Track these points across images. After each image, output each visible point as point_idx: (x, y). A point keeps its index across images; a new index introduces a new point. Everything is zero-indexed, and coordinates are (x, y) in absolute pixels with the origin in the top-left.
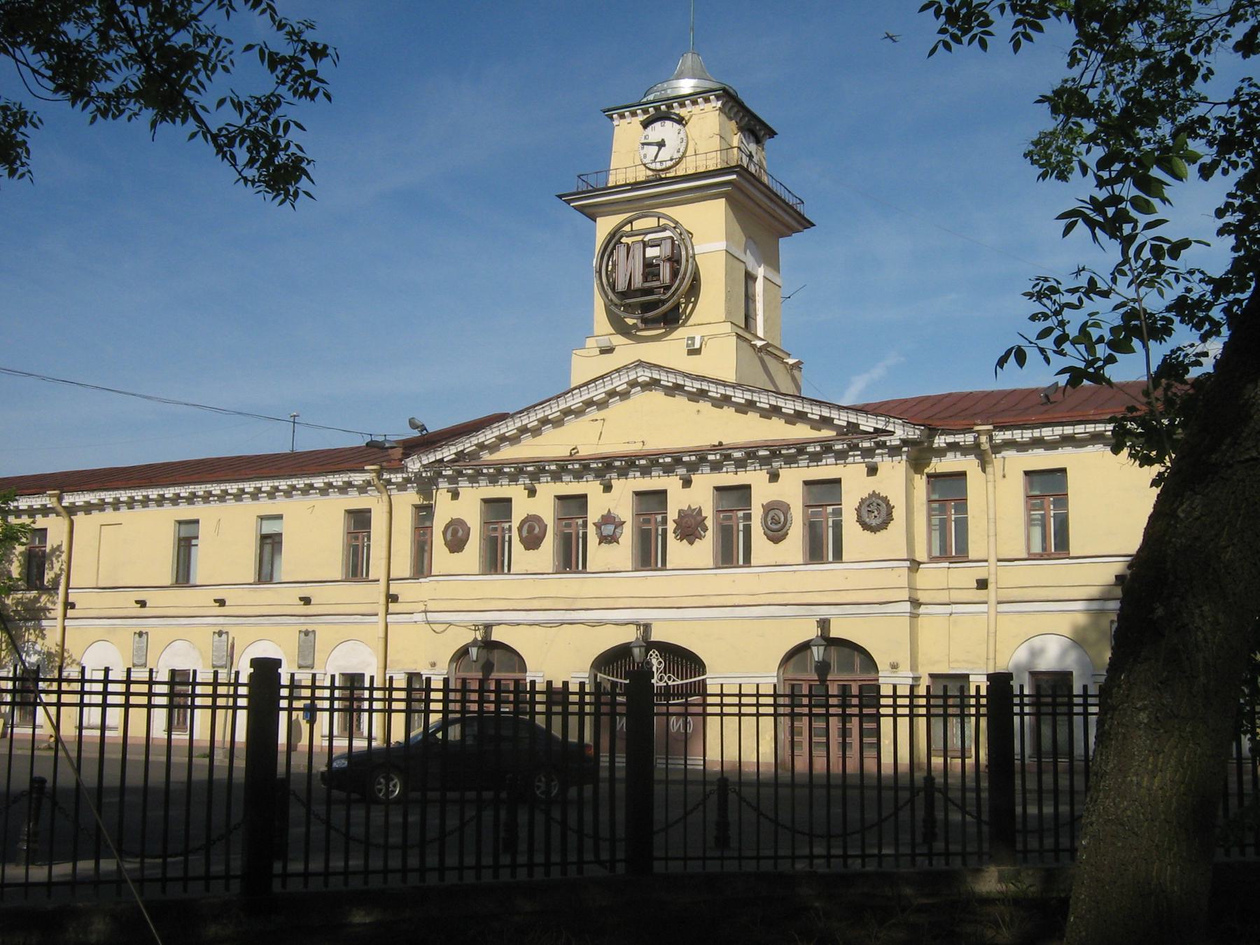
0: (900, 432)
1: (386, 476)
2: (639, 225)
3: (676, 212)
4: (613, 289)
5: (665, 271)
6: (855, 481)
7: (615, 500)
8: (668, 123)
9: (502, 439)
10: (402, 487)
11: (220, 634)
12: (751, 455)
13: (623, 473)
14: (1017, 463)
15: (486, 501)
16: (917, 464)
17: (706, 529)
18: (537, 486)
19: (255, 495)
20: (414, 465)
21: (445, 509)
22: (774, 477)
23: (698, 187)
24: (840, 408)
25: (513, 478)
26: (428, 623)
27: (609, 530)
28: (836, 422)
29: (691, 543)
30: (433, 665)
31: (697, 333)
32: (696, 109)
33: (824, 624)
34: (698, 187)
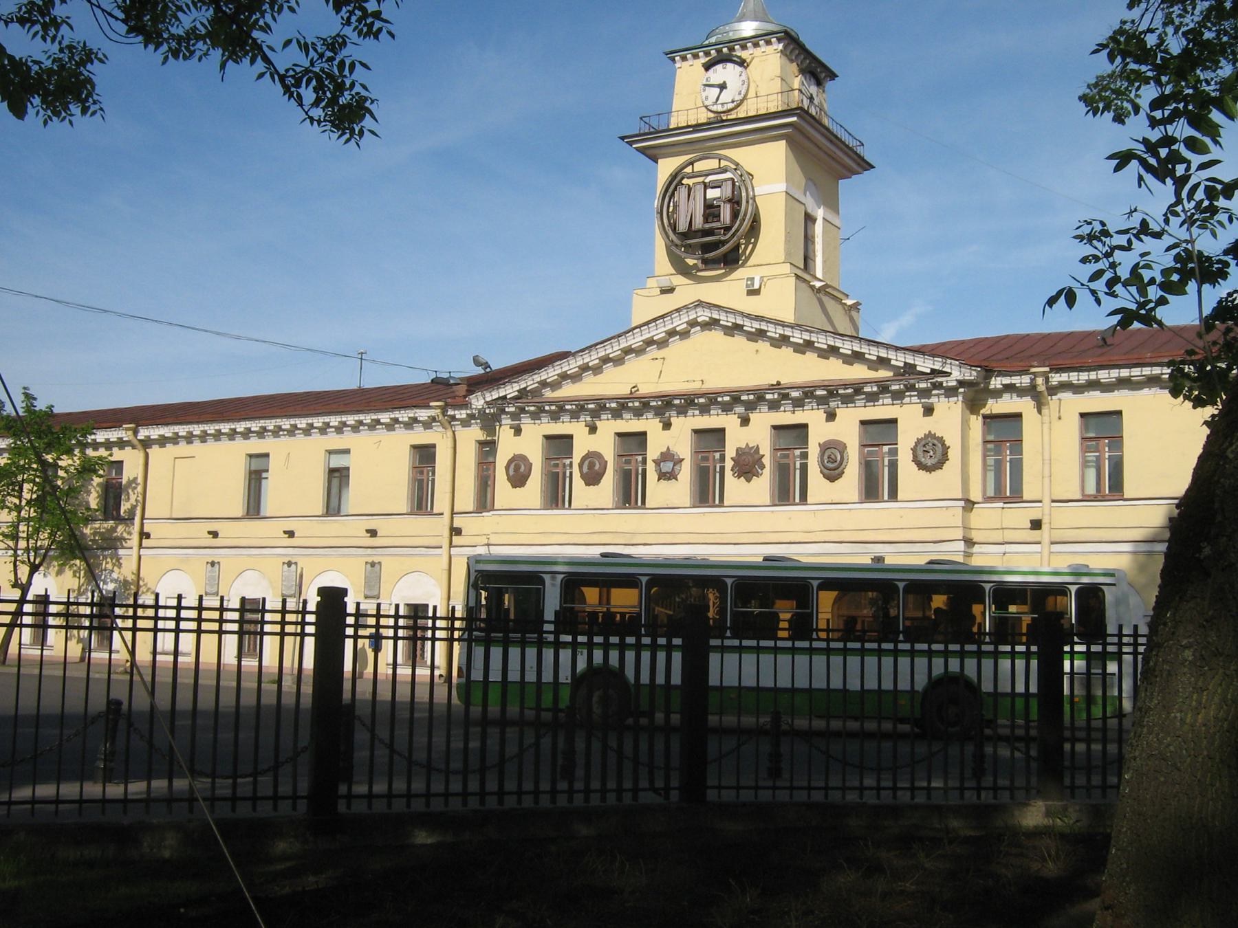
1: (450, 412)
2: (700, 166)
3: (736, 154)
4: (674, 230)
5: (726, 213)
6: (911, 423)
7: (673, 438)
8: (730, 65)
9: (564, 377)
10: (466, 423)
11: (289, 564)
12: (807, 394)
13: (682, 411)
14: (1072, 405)
15: (548, 438)
16: (973, 405)
19: (323, 430)
20: (478, 401)
21: (507, 445)
22: (831, 416)
23: (758, 129)
24: (897, 349)
25: (575, 415)
28: (893, 362)
29: (748, 480)
31: (757, 274)
32: (758, 52)
34: (758, 129)
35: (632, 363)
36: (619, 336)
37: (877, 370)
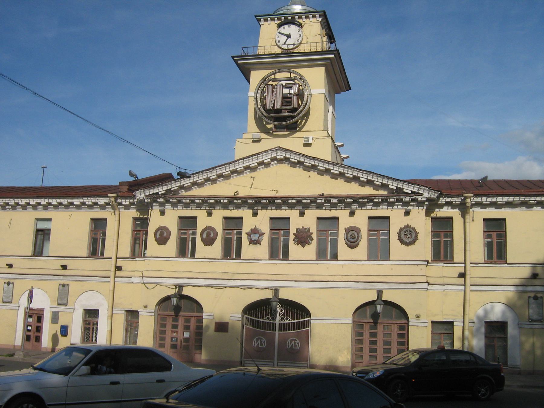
0: (426, 194)
1: (119, 200)
2: (278, 76)
3: (302, 71)
4: (264, 108)
5: (295, 102)
6: (397, 218)
8: (293, 26)
9: (194, 184)
10: (127, 207)
11: (9, 283)
12: (341, 201)
13: (265, 207)
14: (479, 215)
15: (180, 218)
16: (428, 213)
17: (312, 239)
18: (213, 211)
19: (35, 207)
20: (140, 195)
21: (156, 220)
22: (255, 214)
23: (311, 59)
24: (394, 179)
25: (199, 206)
26: (144, 283)
27: (255, 237)
28: (390, 187)
29: (303, 246)
30: (146, 307)
31: (311, 136)
32: (307, 21)
33: (380, 293)
34: (311, 59)
35: (235, 179)
36: (231, 163)
37: (378, 190)
